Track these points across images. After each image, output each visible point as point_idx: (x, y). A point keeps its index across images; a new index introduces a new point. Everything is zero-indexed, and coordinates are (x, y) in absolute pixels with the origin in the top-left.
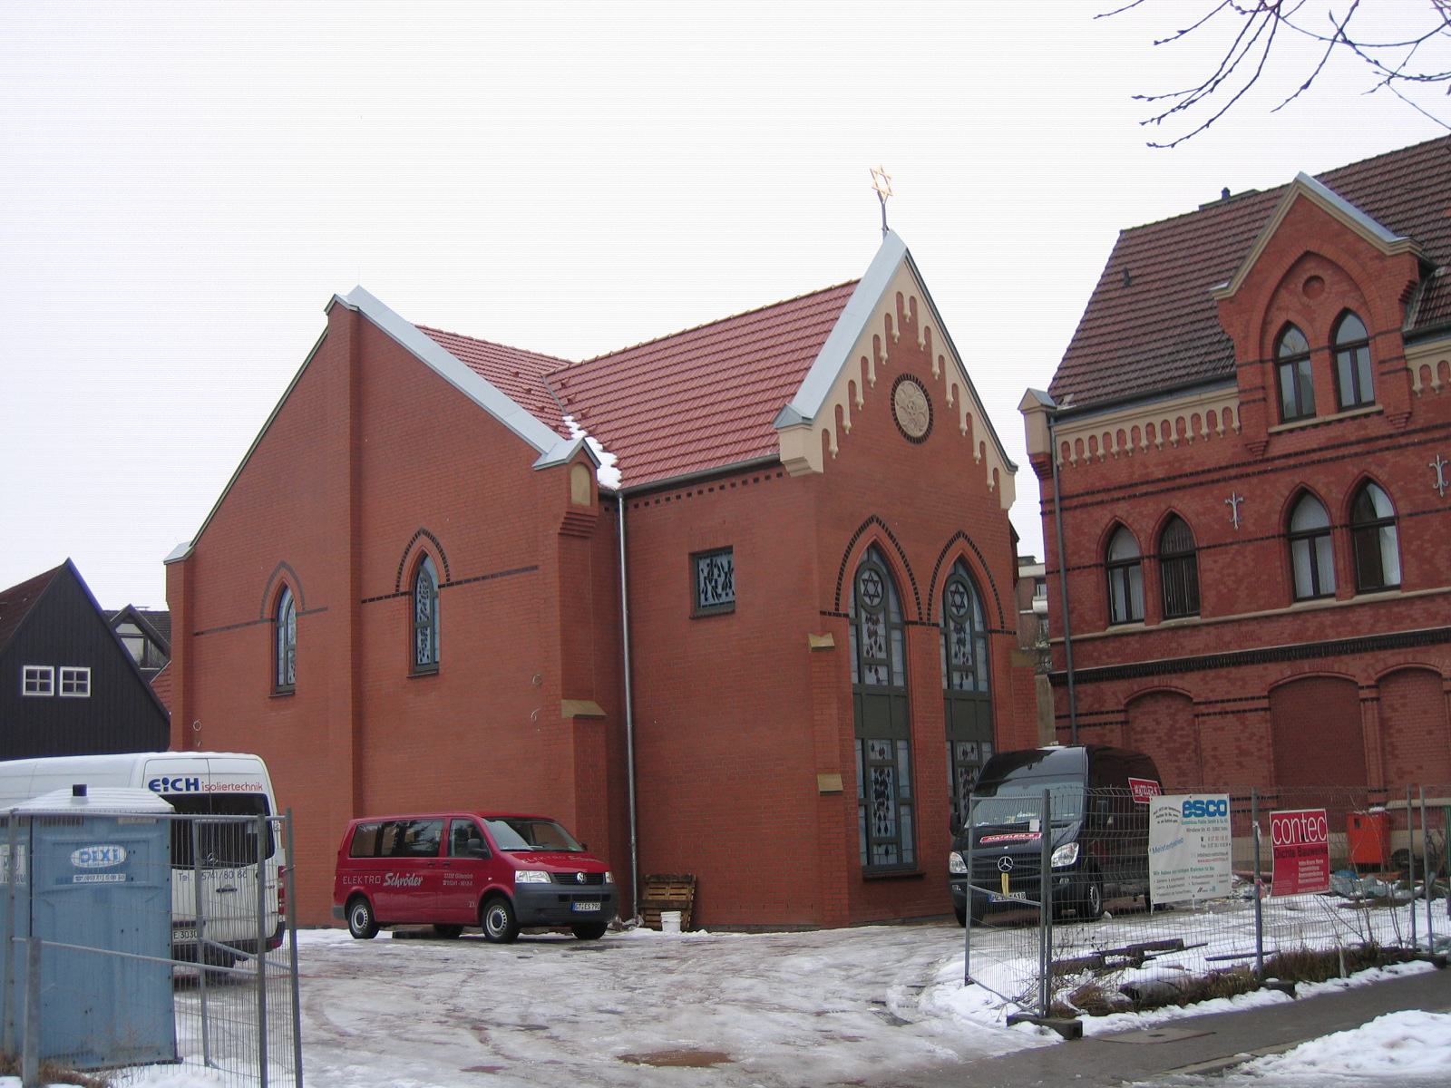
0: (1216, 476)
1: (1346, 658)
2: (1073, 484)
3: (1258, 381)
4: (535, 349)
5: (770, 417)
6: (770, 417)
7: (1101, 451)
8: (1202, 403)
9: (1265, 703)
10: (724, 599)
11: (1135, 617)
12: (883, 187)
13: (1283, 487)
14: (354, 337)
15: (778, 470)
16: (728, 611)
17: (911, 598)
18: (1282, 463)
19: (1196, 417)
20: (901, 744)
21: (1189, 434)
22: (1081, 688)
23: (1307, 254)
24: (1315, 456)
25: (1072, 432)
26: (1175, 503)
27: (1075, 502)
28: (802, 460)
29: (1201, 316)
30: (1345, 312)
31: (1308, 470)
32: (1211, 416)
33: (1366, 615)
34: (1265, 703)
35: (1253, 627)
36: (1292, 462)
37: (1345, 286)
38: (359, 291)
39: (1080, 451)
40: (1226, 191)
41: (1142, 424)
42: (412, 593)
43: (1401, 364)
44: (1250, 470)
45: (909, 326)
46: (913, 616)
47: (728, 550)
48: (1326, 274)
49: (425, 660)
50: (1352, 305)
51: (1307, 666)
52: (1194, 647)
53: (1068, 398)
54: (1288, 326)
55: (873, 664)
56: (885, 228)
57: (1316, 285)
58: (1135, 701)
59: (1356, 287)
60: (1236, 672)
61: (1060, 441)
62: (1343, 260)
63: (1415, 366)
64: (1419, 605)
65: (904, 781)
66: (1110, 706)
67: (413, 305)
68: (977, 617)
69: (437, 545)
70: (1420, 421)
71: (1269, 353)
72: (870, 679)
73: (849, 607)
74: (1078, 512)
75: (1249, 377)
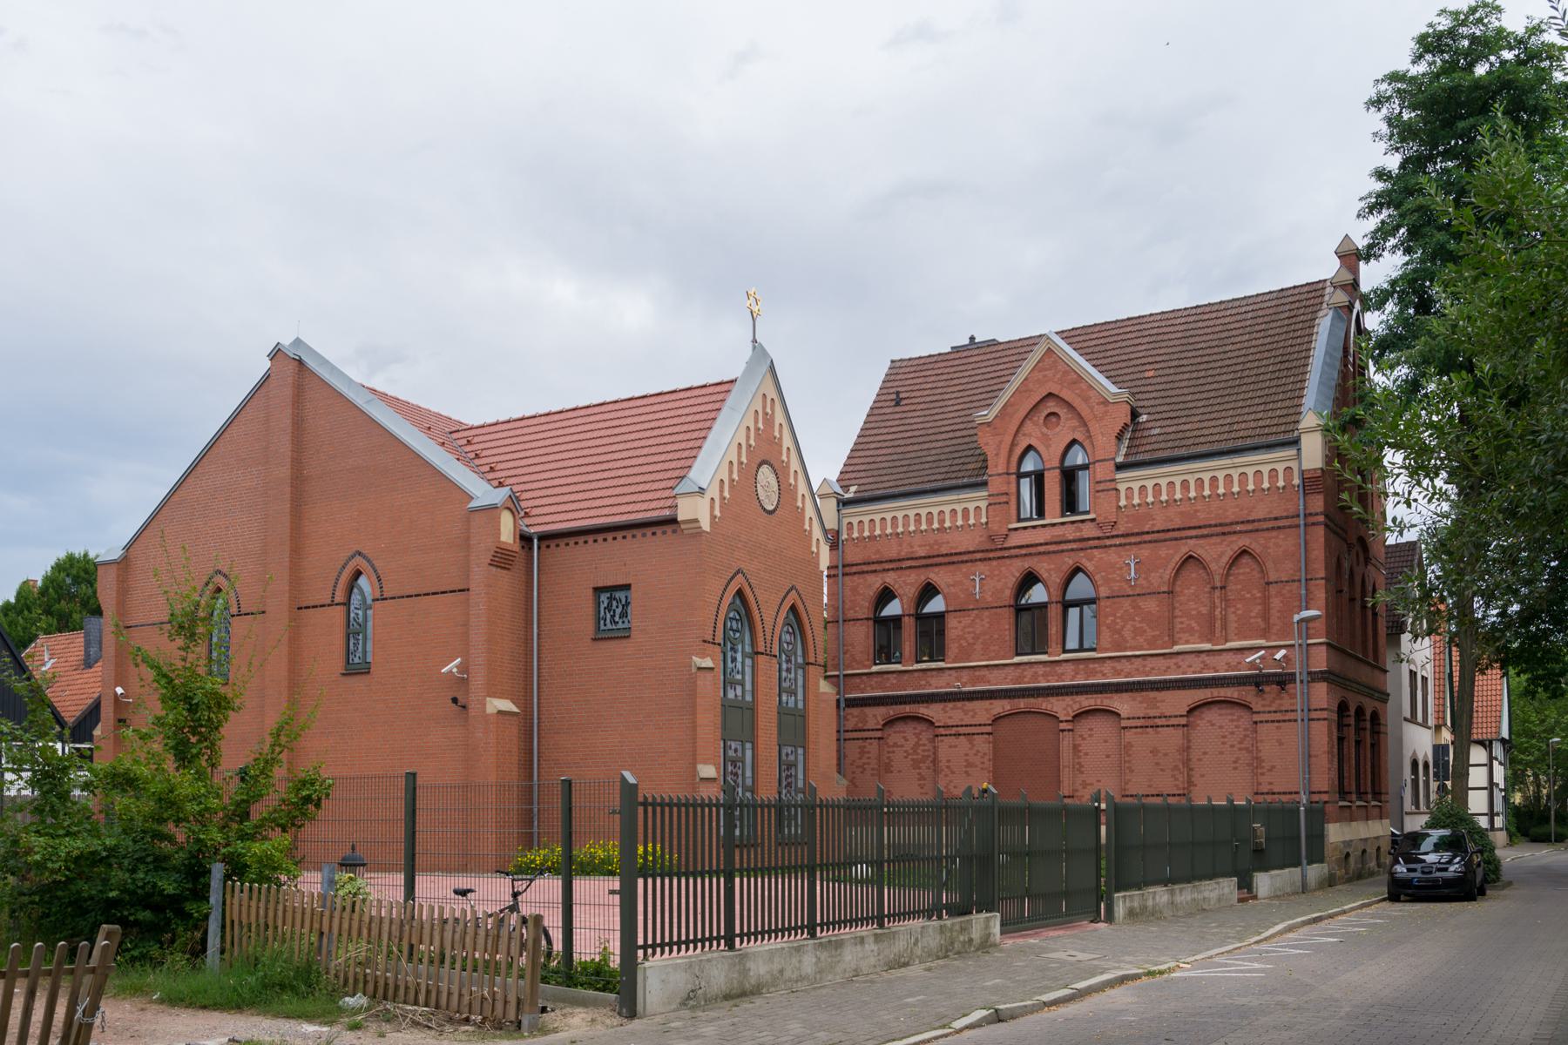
0: (965, 558)
1: (1053, 700)
2: (853, 555)
3: (1004, 489)
4: (434, 409)
5: (670, 483)
6: (670, 483)
7: (878, 532)
8: (959, 501)
9: (989, 729)
10: (620, 625)
11: (1086, 646)
12: (755, 309)
13: (1015, 570)
14: (294, 380)
15: (674, 527)
16: (625, 635)
17: (760, 634)
18: (1013, 552)
19: (954, 511)
20: (748, 745)
21: (947, 524)
22: (849, 710)
23: (1050, 394)
24: (1042, 549)
25: (856, 515)
26: (932, 575)
27: (854, 569)
28: (696, 521)
29: (958, 434)
30: (1074, 442)
31: (1036, 559)
32: (966, 511)
33: (1069, 668)
34: (989, 729)
35: (985, 672)
36: (1024, 551)
37: (1075, 423)
38: (298, 342)
39: (861, 531)
40: (972, 338)
41: (911, 513)
42: (347, 604)
43: (1112, 485)
44: (991, 555)
45: (769, 420)
46: (761, 649)
47: (627, 587)
48: (1062, 412)
49: (356, 660)
50: (1079, 436)
51: (1022, 704)
52: (938, 686)
53: (853, 489)
54: (1030, 448)
55: (734, 684)
56: (754, 341)
57: (1054, 419)
58: (890, 723)
59: (1085, 425)
60: (969, 705)
61: (845, 521)
62: (1077, 402)
63: (1122, 487)
64: (1109, 664)
65: (748, 773)
66: (871, 724)
67: (348, 360)
68: (799, 652)
69: (373, 566)
70: (1121, 529)
71: (1013, 470)
72: (731, 695)
73: (720, 639)
74: (855, 578)
75: (996, 484)
